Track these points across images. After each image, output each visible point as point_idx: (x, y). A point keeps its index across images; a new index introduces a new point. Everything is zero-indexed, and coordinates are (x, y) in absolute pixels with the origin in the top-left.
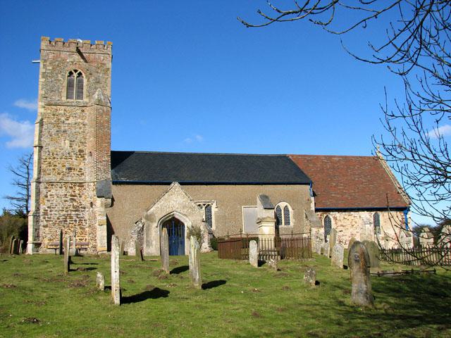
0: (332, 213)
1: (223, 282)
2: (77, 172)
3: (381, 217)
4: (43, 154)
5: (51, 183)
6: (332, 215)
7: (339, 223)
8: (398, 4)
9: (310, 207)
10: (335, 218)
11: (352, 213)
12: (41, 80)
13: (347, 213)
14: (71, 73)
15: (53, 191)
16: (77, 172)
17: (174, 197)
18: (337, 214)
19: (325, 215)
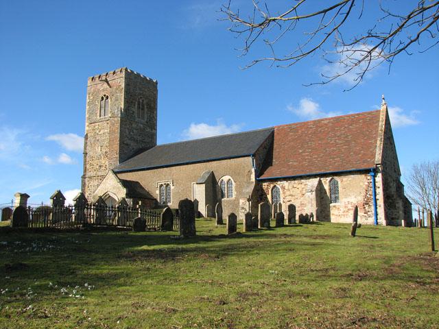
0: (279, 182)
1: (357, 208)
2: (104, 168)
3: (340, 185)
4: (87, 158)
5: (90, 178)
6: (279, 184)
7: (288, 193)
8: (435, 23)
9: (250, 179)
10: (283, 188)
11: (302, 181)
12: (87, 107)
13: (296, 181)
14: (103, 98)
15: (92, 183)
16: (104, 168)
17: (108, 181)
18: (285, 183)
19: (272, 186)
